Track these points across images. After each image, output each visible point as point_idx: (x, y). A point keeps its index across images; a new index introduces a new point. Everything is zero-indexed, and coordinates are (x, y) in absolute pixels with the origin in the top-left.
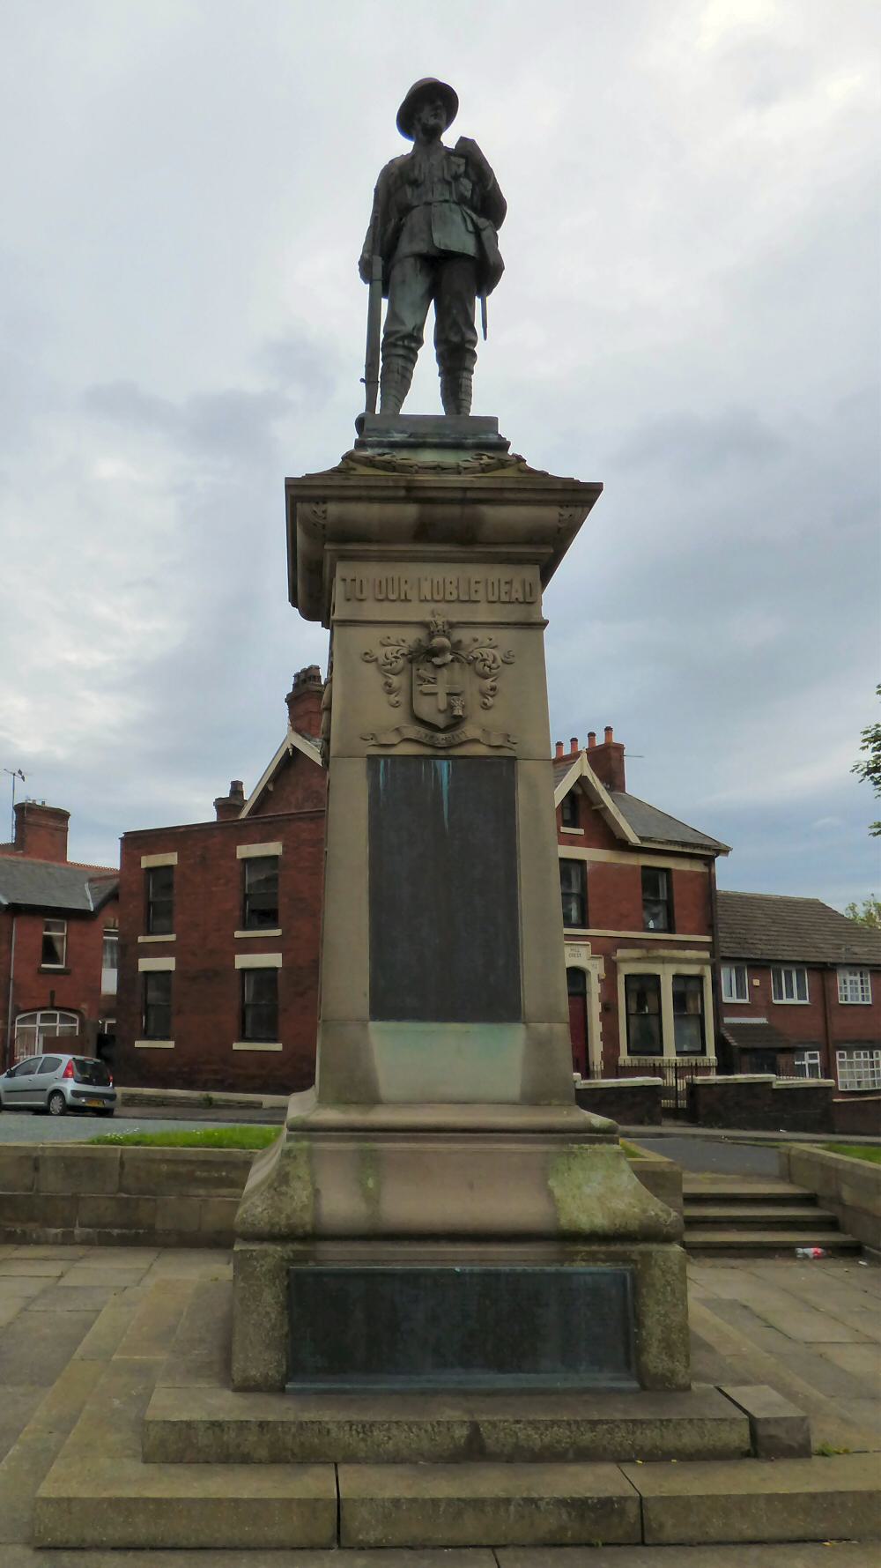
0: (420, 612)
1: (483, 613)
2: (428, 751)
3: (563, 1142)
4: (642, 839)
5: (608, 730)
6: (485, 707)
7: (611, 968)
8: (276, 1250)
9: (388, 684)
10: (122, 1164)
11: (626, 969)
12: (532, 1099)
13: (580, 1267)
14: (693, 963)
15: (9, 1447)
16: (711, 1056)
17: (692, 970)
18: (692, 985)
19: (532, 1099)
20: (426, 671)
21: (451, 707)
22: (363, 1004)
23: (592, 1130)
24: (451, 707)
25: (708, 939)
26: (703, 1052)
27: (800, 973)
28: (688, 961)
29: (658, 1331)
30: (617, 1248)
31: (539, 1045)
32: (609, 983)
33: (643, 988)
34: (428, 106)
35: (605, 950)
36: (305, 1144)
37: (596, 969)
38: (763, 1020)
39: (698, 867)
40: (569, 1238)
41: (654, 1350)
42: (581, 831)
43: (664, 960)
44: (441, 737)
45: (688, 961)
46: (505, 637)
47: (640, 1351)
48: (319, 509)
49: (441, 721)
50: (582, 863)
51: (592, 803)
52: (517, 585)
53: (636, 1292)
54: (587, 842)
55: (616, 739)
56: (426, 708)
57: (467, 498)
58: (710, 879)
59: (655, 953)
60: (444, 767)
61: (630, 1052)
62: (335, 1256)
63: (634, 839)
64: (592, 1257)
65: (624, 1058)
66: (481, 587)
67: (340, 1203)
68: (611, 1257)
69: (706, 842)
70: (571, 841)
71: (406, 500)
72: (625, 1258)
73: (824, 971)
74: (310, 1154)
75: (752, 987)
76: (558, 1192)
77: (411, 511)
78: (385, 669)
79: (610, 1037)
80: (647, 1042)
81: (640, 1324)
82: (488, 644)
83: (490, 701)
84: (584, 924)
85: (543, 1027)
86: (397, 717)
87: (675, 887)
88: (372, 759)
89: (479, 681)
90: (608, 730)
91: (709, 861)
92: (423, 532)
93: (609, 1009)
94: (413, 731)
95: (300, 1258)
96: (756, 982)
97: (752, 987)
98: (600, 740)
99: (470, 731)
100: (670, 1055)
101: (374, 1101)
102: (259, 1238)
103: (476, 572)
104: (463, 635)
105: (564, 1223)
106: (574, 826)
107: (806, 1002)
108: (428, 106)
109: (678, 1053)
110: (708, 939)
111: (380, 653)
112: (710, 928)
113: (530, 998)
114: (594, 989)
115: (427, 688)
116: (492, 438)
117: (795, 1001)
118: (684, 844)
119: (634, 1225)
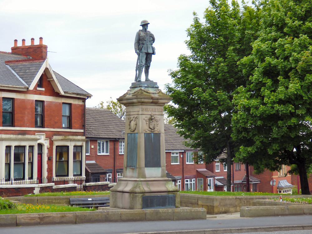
0: (150, 113)
1: (157, 113)
2: (151, 132)
3: (166, 181)
4: (65, 92)
5: (41, 38)
6: (157, 126)
7: (51, 143)
8: (141, 194)
9: (147, 123)
10: (37, 200)
11: (56, 144)
12: (162, 177)
13: (170, 195)
14: (80, 140)
15: (305, 134)
16: (84, 176)
17: (79, 144)
18: (79, 149)
19: (162, 177)
20: (151, 122)
21: (154, 127)
22: (144, 166)
23: (170, 180)
24: (154, 127)
25: (82, 131)
26: (81, 175)
27: (107, 142)
28: (79, 140)
29: (177, 202)
30: (173, 193)
31: (163, 170)
32: (50, 150)
33: (62, 151)
34: (145, 25)
35: (49, 136)
36: (141, 183)
37: (46, 144)
38: (93, 162)
39: (80, 103)
40: (169, 192)
41: (177, 203)
42: (43, 89)
43: (71, 140)
44: (153, 130)
45: (79, 140)
46: (159, 116)
47: (176, 204)
48: (141, 100)
49: (153, 128)
50: (43, 102)
51: (48, 78)
52: (161, 109)
53: (175, 197)
54: (45, 94)
55: (44, 43)
56: (151, 127)
57: (158, 99)
58: (84, 105)
59: (68, 137)
60: (152, 134)
61: (56, 176)
62: (147, 195)
63: (62, 93)
64: (171, 194)
65: (55, 178)
66: (157, 110)
67: (146, 189)
68: (173, 194)
69: (84, 93)
70: (40, 93)
71: (151, 99)
72: (174, 194)
73: (115, 141)
74: (141, 184)
75: (91, 148)
76: (167, 187)
77: (151, 100)
78: (146, 121)
79: (50, 170)
80: (63, 171)
81: (175, 201)
82: (158, 117)
83: (158, 125)
84: (43, 126)
85: (163, 168)
86: (147, 128)
87: (73, 111)
88: (145, 133)
89: (156, 122)
90: (41, 38)
91: (84, 100)
92: (152, 103)
93: (50, 159)
94: (150, 130)
95: (143, 195)
96: (93, 147)
97: (91, 148)
98: (37, 43)
99: (156, 129)
100: (71, 176)
101: (145, 178)
102: (139, 193)
103: (156, 107)
104: (155, 116)
105: (169, 190)
106: (41, 87)
107: (108, 154)
108: (145, 25)
109: (74, 175)
110: (82, 131)
111: (146, 119)
112: (83, 127)
113: (162, 164)
114: (45, 151)
115: (151, 124)
116: (156, 86)
117: (105, 154)
118: (78, 94)
119: (175, 190)
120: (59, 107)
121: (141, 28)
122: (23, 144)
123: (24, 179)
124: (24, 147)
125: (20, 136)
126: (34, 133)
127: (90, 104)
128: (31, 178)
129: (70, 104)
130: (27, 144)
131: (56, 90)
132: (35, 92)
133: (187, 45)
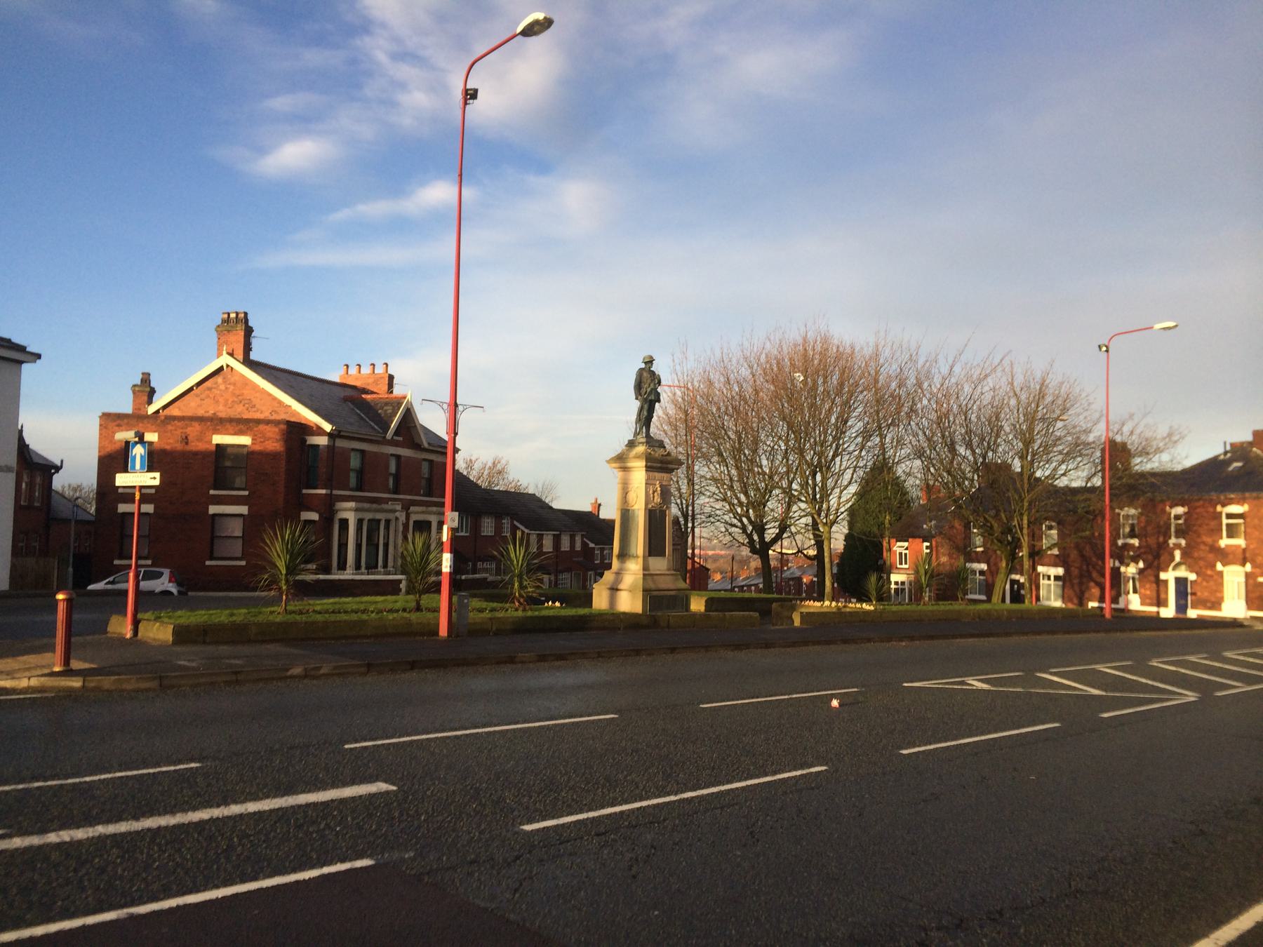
7: (408, 518)
11: (414, 518)
34: (649, 362)
63: (426, 445)
84: (396, 491)
93: (358, 547)
120: (419, 462)
121: (643, 366)
122: (378, 516)
123: (376, 567)
124: (379, 521)
125: (375, 506)
126: (386, 501)
127: (58, 482)
128: (385, 566)
129: (431, 462)
130: (381, 516)
131: (417, 441)
132: (392, 443)
133: (994, 423)
